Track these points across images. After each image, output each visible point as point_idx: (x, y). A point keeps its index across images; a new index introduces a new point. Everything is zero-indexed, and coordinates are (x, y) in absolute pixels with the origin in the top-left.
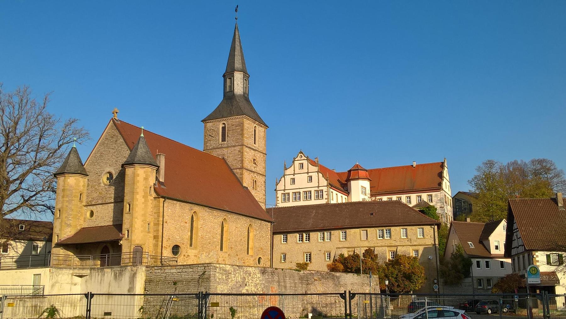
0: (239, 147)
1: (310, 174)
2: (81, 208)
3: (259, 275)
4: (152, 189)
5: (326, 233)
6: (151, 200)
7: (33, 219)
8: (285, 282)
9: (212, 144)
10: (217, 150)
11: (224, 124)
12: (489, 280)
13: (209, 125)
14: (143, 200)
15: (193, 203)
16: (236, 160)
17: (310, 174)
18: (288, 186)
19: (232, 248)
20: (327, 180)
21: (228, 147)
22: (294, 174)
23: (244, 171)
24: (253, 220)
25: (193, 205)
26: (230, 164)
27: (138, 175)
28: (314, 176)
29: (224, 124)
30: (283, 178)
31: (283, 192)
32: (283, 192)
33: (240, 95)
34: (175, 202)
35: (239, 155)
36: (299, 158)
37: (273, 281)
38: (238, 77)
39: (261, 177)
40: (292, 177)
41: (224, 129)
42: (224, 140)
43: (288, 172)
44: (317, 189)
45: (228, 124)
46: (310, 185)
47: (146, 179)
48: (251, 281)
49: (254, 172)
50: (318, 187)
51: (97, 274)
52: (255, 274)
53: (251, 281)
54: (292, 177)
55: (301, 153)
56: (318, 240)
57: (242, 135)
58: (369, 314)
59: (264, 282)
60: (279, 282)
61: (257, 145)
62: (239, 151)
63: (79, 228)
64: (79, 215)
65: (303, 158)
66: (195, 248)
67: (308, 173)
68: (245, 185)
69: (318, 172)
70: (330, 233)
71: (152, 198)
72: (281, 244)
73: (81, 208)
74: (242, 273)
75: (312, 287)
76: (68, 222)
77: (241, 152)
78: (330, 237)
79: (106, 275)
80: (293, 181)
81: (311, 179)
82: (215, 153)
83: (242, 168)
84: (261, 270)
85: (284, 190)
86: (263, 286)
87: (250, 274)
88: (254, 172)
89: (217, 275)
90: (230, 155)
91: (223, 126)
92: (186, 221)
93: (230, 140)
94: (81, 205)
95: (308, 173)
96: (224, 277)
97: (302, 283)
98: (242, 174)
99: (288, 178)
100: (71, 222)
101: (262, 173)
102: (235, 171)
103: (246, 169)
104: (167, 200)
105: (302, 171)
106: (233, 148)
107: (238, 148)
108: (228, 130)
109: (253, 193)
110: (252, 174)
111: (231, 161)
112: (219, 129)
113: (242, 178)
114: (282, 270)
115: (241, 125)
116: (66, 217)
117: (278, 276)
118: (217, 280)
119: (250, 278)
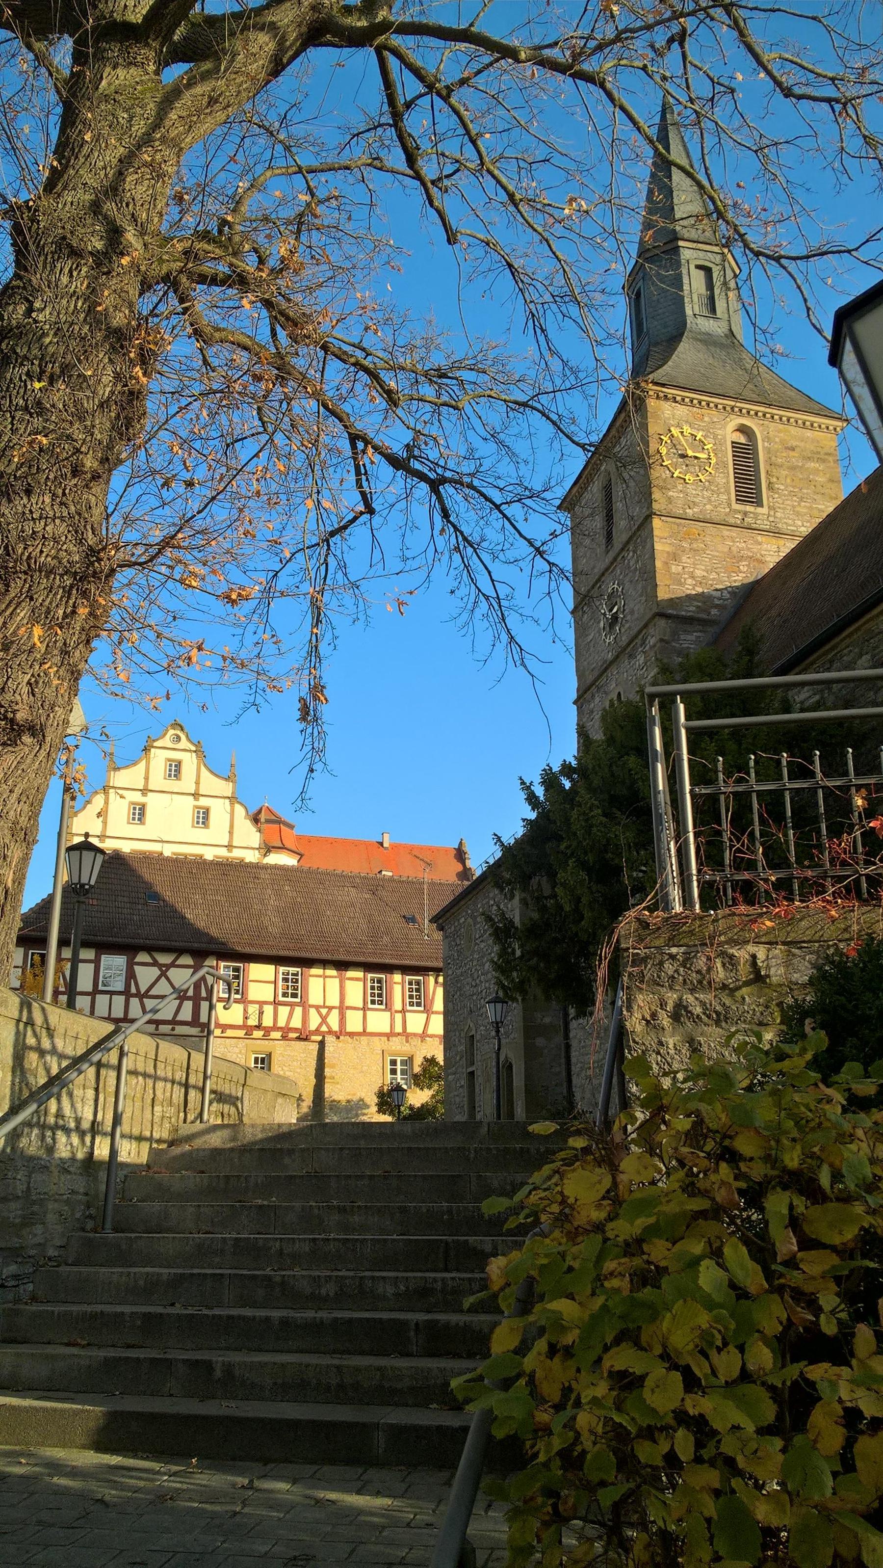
1: (203, 802)
7: (140, 1410)
12: (275, 1364)
17: (203, 802)
22: (145, 791)
28: (219, 811)
33: (101, 1163)
36: (166, 741)
43: (121, 778)
46: (201, 835)
54: (137, 797)
58: (681, 243)
65: (184, 743)
69: (233, 799)
80: (139, 813)
81: (203, 818)
95: (196, 795)
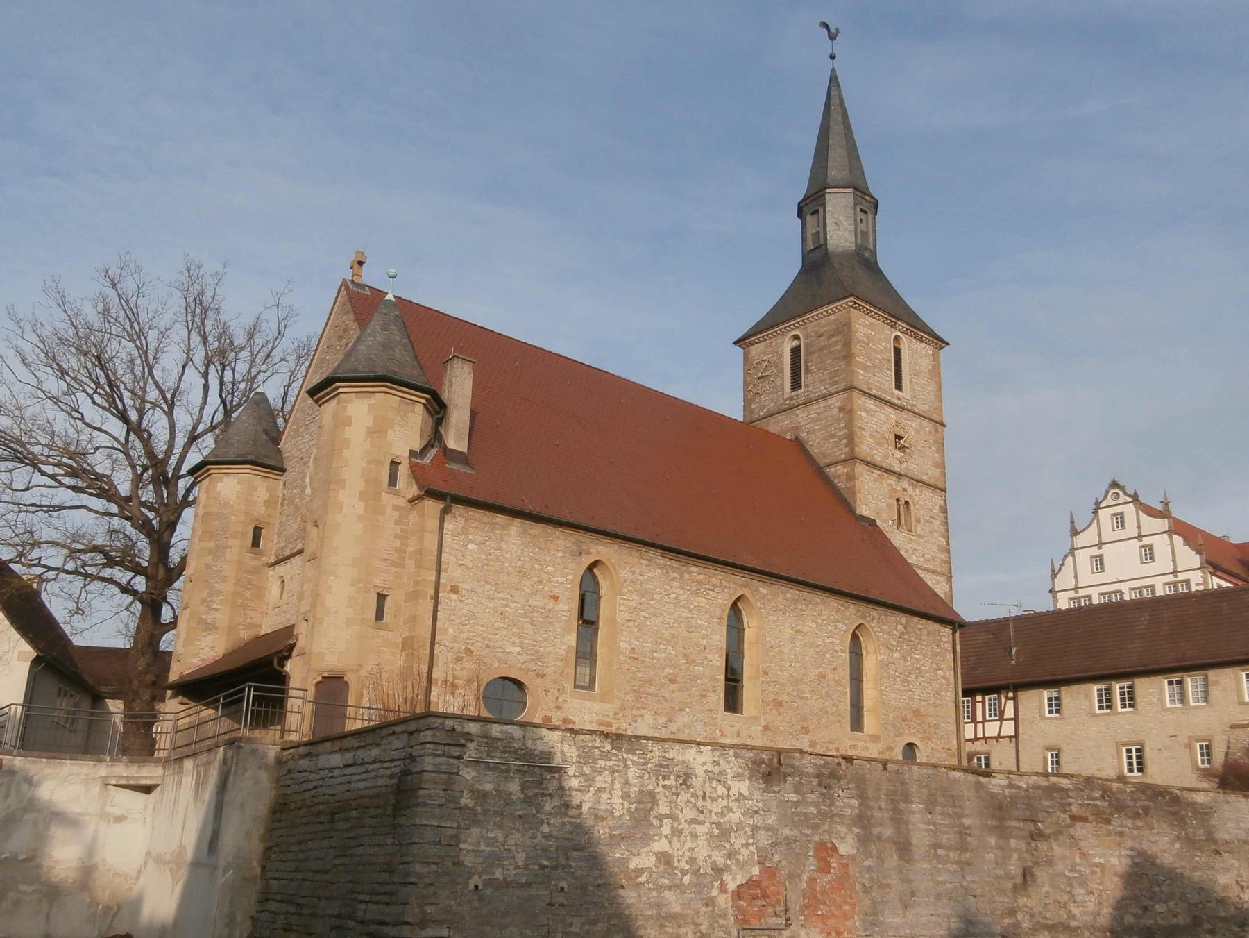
0: (840, 396)
1: (1146, 541)
2: (256, 571)
3: (743, 787)
4: (403, 470)
5: (1189, 681)
6: (395, 508)
8: (899, 819)
9: (768, 402)
10: (779, 417)
11: (796, 337)
13: (757, 349)
14: (360, 508)
15: (586, 529)
16: (832, 436)
17: (1146, 541)
18: (1086, 577)
19: (779, 704)
20: (1198, 552)
21: (808, 402)
22: (1100, 545)
23: (860, 469)
24: (874, 612)
25: (588, 538)
26: (815, 452)
27: (348, 422)
29: (796, 337)
30: (1070, 558)
31: (1072, 594)
32: (1072, 594)
33: (845, 255)
34: (500, 519)
35: (839, 420)
36: (1109, 501)
37: (830, 816)
38: (838, 205)
39: (928, 493)
40: (1095, 551)
41: (796, 352)
42: (796, 384)
44: (1170, 578)
45: (807, 337)
46: (1150, 569)
47: (377, 432)
48: (689, 813)
49: (899, 475)
50: (1175, 573)
51: (421, 792)
52: (720, 777)
53: (689, 813)
54: (1095, 551)
55: (1114, 485)
56: (1162, 701)
57: (848, 357)
59: (771, 820)
60: (863, 821)
61: (906, 395)
62: (841, 409)
63: (245, 635)
64: (248, 594)
65: (1123, 498)
66: (605, 697)
67: (1140, 537)
68: (863, 510)
70: (1206, 678)
71: (402, 502)
72: (1043, 718)
73: (256, 571)
74: (632, 773)
75: (1057, 850)
76: (209, 618)
77: (847, 412)
78: (1206, 693)
79: (184, 780)
80: (1099, 563)
81: (1149, 553)
82: (774, 426)
83: (852, 458)
84: (757, 763)
85: (1076, 589)
86: (764, 839)
87: (686, 780)
88: (899, 475)
89: (468, 774)
90: (814, 426)
91: (795, 343)
92: (557, 591)
93: (813, 382)
94: (256, 563)
95: (1140, 537)
96: (514, 787)
97: (1002, 832)
98: (851, 478)
99: (1083, 557)
100: (217, 615)
101: (931, 481)
102: (831, 471)
103: (866, 463)
104: (458, 509)
105: (1122, 534)
106: (822, 404)
107: (835, 402)
108: (806, 355)
109: (898, 539)
110: (892, 480)
111: (818, 445)
112: (781, 356)
113: (852, 491)
114: (885, 764)
115: (844, 330)
116: (203, 601)
117: (862, 796)
118: (466, 800)
119: (685, 796)
